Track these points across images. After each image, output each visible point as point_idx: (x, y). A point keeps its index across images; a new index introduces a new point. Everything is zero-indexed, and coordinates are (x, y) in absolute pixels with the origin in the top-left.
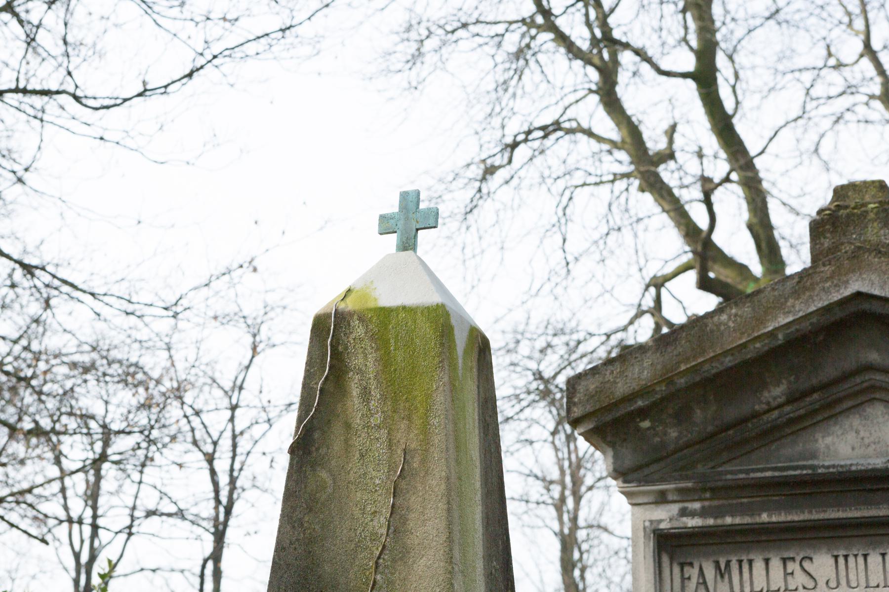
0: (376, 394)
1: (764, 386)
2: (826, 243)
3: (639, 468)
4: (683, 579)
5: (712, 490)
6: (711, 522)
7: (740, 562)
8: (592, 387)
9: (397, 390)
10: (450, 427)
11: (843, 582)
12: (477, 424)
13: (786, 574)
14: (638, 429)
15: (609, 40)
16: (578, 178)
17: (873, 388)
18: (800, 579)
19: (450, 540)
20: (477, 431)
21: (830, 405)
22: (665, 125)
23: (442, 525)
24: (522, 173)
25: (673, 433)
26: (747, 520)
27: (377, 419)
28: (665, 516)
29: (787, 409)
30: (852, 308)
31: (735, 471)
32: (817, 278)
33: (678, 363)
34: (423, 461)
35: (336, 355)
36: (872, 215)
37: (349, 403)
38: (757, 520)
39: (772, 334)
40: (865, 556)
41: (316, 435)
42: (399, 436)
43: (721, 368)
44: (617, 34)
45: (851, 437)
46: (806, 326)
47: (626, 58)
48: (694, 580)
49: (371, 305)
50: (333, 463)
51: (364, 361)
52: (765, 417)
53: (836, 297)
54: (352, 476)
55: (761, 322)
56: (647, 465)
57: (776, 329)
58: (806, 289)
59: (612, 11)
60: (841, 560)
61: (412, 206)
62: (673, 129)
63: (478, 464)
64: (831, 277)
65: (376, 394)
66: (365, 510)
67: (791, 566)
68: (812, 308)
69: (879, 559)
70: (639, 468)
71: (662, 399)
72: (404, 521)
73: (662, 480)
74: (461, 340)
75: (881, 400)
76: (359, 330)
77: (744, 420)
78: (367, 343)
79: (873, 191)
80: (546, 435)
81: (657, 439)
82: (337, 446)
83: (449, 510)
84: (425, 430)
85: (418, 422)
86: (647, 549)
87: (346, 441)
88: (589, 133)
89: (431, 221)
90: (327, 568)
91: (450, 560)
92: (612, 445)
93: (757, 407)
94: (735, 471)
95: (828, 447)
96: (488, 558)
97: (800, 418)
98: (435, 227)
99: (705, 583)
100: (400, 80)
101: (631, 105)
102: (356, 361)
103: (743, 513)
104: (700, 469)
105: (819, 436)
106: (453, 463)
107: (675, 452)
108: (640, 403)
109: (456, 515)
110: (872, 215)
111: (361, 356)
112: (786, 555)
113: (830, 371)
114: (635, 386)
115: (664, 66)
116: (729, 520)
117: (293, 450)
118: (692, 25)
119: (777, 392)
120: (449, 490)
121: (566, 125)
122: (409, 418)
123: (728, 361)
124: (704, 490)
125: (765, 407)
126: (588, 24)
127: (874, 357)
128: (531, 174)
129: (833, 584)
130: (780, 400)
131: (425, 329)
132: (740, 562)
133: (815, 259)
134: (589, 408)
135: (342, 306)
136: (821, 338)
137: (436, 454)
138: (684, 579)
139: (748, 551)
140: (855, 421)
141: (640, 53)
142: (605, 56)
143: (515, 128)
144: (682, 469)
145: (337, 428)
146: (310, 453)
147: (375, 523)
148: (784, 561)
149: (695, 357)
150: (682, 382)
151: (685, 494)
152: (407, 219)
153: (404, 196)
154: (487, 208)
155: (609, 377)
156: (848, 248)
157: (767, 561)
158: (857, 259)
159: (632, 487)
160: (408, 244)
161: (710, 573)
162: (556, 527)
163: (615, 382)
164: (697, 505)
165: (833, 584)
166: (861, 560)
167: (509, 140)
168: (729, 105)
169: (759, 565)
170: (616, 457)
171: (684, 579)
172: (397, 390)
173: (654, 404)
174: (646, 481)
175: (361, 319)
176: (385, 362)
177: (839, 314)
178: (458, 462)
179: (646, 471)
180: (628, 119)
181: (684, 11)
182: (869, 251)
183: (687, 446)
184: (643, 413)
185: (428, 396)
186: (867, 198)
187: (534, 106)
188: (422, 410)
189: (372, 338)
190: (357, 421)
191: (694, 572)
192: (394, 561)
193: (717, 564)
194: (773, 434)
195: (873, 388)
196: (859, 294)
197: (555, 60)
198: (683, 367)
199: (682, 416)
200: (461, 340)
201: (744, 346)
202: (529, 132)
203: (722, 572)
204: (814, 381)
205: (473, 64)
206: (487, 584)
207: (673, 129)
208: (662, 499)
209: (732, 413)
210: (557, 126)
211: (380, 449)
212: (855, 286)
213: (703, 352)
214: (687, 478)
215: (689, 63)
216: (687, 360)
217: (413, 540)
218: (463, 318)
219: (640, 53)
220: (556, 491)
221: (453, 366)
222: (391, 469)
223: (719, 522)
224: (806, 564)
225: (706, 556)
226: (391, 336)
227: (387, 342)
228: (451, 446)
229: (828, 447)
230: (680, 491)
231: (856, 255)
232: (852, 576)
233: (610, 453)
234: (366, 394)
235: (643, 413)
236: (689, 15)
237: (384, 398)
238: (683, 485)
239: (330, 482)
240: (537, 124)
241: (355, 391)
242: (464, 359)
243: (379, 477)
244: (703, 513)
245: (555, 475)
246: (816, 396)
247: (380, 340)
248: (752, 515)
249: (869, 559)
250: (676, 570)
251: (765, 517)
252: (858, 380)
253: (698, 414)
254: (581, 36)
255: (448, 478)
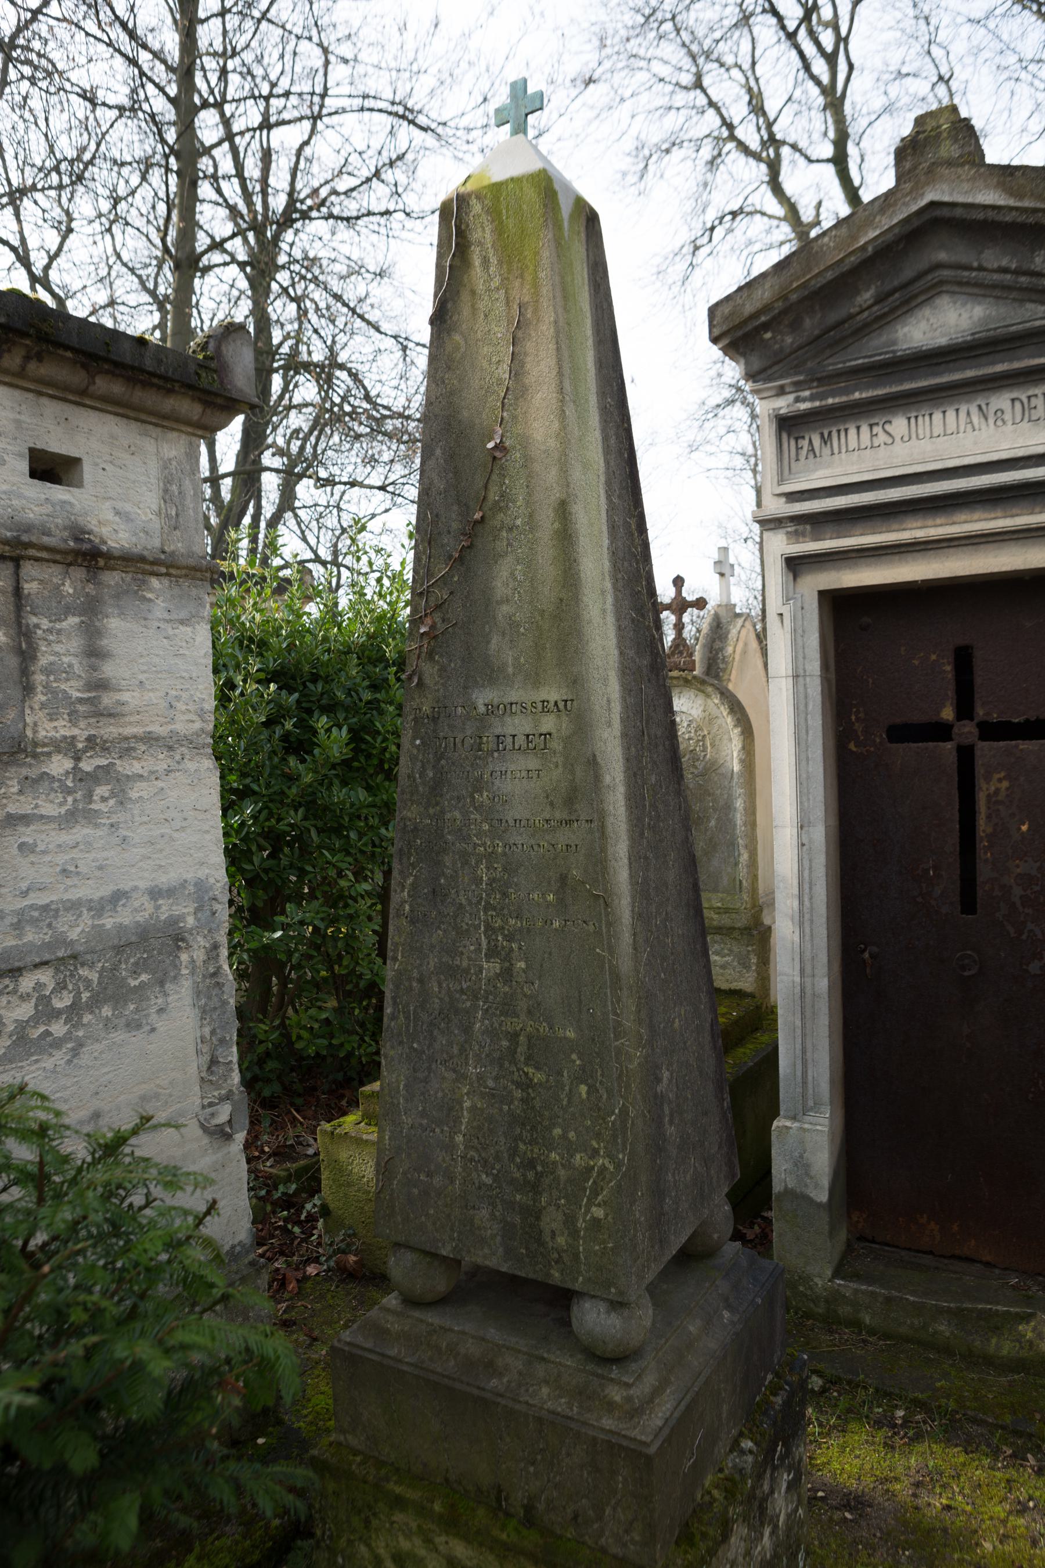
0: (494, 260)
1: (857, 292)
2: (908, 165)
3: (764, 370)
4: (797, 449)
5: (819, 380)
6: (817, 404)
7: (839, 431)
8: (727, 311)
9: (511, 254)
10: (557, 279)
11: (914, 436)
12: (586, 281)
13: (872, 436)
14: (762, 340)
15: (772, 141)
16: (757, 247)
17: (941, 283)
18: (882, 437)
19: (560, 374)
20: (586, 288)
21: (907, 301)
22: (814, 203)
23: (553, 362)
24: (718, 248)
25: (789, 340)
26: (844, 399)
27: (496, 282)
28: (784, 404)
29: (875, 308)
30: (926, 217)
31: (836, 363)
32: (899, 195)
33: (791, 282)
34: (536, 311)
35: (460, 233)
36: (945, 135)
37: (473, 273)
38: (852, 397)
39: (863, 248)
40: (931, 415)
41: (449, 305)
42: (515, 293)
43: (824, 281)
44: (778, 137)
45: (923, 325)
46: (890, 237)
47: (785, 151)
48: (805, 449)
49: (486, 183)
50: (464, 326)
51: (482, 234)
52: (858, 318)
53: (914, 208)
54: (479, 335)
55: (854, 238)
56: (770, 367)
57: (866, 243)
58: (890, 206)
59: (775, 120)
60: (913, 420)
61: (520, 93)
62: (819, 204)
63: (588, 315)
64: (911, 192)
65: (494, 260)
66: (491, 361)
67: (875, 430)
68: (895, 221)
69: (941, 415)
70: (764, 370)
71: (780, 313)
72: (522, 364)
73: (781, 377)
74: (566, 207)
75: (947, 292)
76: (476, 207)
77: (843, 322)
78: (484, 218)
79: (946, 115)
80: (746, 427)
81: (777, 346)
82: (466, 311)
83: (558, 349)
84: (536, 285)
85: (528, 278)
86: (769, 431)
87: (473, 306)
88: (763, 214)
89: (538, 104)
90: (465, 414)
91: (561, 390)
92: (743, 355)
93: (852, 310)
94: (836, 363)
95: (905, 335)
96: (602, 394)
97: (885, 315)
98: (541, 109)
99: (813, 450)
100: (634, 190)
101: (790, 187)
102: (475, 236)
103: (841, 395)
104: (809, 364)
105: (899, 327)
106: (560, 310)
107: (791, 354)
108: (763, 319)
109: (566, 354)
110: (945, 135)
111: (479, 230)
112: (873, 421)
113: (908, 273)
114: (758, 305)
115: (814, 158)
116: (830, 401)
117: (432, 321)
118: (830, 121)
119: (867, 296)
120: (557, 332)
121: (747, 209)
122: (522, 276)
123: (830, 275)
124: (812, 380)
125: (857, 309)
126: (759, 129)
127: (942, 256)
128: (725, 247)
129: (906, 438)
130: (870, 302)
131: (531, 194)
132: (839, 431)
133: (899, 178)
134: (725, 328)
135: (462, 190)
136: (901, 246)
137: (545, 303)
138: (798, 449)
139: (845, 422)
140: (927, 311)
141: (794, 147)
142: (771, 153)
143: (711, 216)
144: (796, 366)
145: (465, 296)
146: (445, 322)
147: (500, 370)
148: (871, 426)
149: (804, 275)
150: (794, 297)
151: (798, 386)
152: (517, 106)
153: (514, 85)
154: (698, 275)
155: (739, 301)
156: (925, 165)
157: (858, 428)
158: (931, 175)
159: (759, 386)
160: (520, 128)
161: (817, 441)
162: (753, 483)
163: (743, 305)
164: (807, 393)
165: (906, 438)
166: (927, 418)
167: (709, 225)
168: (856, 183)
169: (852, 432)
170: (746, 364)
171: (798, 449)
172: (511, 254)
173: (774, 318)
174: (770, 379)
175: (478, 197)
176: (500, 230)
177: (916, 223)
178: (566, 310)
179: (769, 372)
180: (788, 200)
181: (824, 109)
182: (941, 164)
183: (800, 348)
184: (765, 327)
185: (537, 253)
186: (942, 121)
187: (723, 199)
188: (531, 268)
189: (488, 212)
190: (480, 287)
191: (805, 443)
192: (517, 399)
193: (822, 434)
194: (865, 330)
195: (941, 283)
196: (932, 204)
197: (735, 160)
198: (795, 285)
199: (795, 326)
200: (566, 207)
201: (842, 260)
202: (722, 217)
203: (826, 440)
204: (896, 283)
205: (682, 170)
206: (601, 415)
207: (819, 204)
208: (781, 392)
209: (833, 317)
210: (741, 210)
211: (500, 307)
212: (930, 196)
213: (810, 270)
214: (796, 374)
215: (827, 150)
216: (798, 278)
217: (530, 380)
218: (568, 187)
219: (794, 147)
220: (753, 460)
221: (558, 225)
222: (510, 322)
223: (824, 403)
224: (887, 427)
225: (814, 430)
226: (503, 207)
227: (500, 214)
228: (559, 294)
229: (905, 335)
230: (796, 384)
231: (930, 171)
232: (920, 431)
233: (742, 361)
234: (486, 262)
235: (765, 327)
236: (828, 114)
237: (500, 262)
238: (796, 379)
239: (462, 343)
240: (727, 211)
241: (477, 262)
242: (570, 222)
243: (500, 331)
244: (812, 398)
245: (750, 450)
246: (897, 295)
247: (494, 213)
248: (847, 395)
249: (934, 417)
250: (793, 442)
251: (857, 395)
252: (930, 277)
253: (808, 322)
254: (754, 145)
255: (556, 322)
